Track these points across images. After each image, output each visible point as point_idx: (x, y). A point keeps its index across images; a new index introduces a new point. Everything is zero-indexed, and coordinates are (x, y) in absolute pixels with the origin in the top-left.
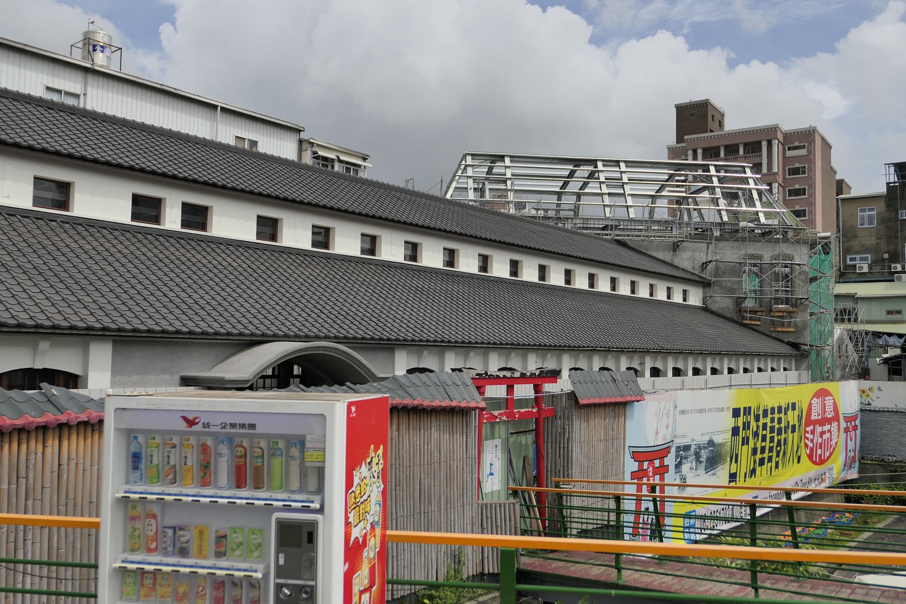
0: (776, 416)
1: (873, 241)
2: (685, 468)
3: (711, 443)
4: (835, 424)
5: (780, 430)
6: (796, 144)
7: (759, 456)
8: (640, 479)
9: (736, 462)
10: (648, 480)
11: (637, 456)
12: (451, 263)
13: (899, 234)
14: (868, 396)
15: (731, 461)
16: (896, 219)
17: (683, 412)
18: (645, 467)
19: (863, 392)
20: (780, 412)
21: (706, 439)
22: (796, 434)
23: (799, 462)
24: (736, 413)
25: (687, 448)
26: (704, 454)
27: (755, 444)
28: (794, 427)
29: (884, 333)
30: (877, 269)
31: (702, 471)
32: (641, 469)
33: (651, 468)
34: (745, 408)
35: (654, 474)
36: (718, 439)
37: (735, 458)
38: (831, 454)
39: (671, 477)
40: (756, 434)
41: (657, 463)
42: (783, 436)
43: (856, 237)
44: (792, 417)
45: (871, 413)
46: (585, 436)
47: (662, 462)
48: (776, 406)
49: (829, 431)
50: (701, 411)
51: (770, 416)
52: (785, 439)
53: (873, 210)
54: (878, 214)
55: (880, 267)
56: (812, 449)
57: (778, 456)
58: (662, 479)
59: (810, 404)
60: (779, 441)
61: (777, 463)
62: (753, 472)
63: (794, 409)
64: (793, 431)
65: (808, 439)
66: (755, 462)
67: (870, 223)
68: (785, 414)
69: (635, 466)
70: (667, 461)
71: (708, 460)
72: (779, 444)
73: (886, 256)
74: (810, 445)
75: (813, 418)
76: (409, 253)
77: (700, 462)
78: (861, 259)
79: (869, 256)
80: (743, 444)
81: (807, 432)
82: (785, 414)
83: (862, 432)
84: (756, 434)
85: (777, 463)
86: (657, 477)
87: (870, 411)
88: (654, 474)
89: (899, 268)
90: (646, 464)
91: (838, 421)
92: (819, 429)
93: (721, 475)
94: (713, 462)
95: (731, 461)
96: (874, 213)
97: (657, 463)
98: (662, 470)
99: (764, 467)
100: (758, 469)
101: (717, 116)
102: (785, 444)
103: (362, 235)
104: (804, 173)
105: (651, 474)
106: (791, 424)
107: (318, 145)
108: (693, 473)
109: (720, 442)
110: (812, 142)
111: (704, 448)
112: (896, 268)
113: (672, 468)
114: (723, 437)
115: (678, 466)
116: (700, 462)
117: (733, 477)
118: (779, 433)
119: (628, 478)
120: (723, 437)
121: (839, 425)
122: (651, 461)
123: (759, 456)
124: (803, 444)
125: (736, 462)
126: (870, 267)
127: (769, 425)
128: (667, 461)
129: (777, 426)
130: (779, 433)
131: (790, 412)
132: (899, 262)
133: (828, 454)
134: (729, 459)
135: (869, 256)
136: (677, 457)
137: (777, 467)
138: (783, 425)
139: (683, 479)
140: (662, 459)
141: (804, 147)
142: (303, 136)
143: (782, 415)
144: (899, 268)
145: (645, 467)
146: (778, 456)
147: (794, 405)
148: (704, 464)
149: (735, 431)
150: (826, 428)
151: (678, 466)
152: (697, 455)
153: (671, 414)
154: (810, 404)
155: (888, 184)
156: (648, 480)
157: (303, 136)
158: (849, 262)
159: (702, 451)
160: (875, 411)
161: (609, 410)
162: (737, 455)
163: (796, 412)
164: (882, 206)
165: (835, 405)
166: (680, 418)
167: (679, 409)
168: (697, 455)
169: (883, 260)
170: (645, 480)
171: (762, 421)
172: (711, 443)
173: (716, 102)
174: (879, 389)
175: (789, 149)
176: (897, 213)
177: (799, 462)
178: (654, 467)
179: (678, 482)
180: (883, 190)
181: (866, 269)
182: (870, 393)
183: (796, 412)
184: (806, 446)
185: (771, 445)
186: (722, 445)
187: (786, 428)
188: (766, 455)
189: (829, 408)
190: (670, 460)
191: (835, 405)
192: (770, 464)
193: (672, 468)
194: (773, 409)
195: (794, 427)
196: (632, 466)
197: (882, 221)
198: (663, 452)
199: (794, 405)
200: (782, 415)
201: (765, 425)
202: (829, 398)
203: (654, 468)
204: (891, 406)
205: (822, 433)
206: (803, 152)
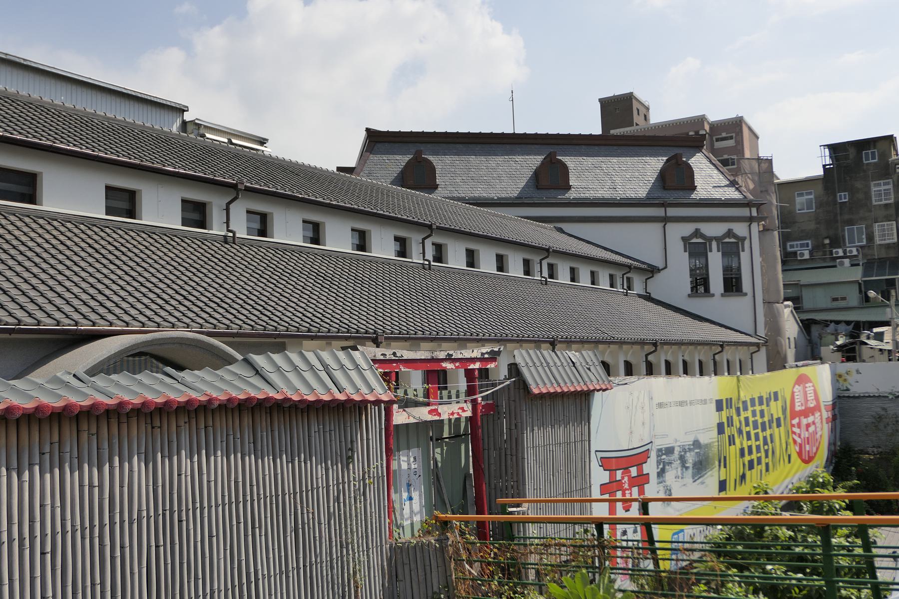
0: (758, 408)
1: (812, 226)
2: (670, 476)
3: (696, 444)
4: (817, 414)
5: (763, 424)
6: (724, 135)
7: (747, 458)
8: (612, 493)
9: (725, 466)
10: (624, 494)
11: (606, 463)
12: (362, 246)
13: (839, 218)
14: (845, 380)
15: (720, 466)
16: (835, 201)
17: (660, 405)
18: (619, 477)
19: (840, 376)
20: (761, 403)
21: (689, 440)
22: (782, 428)
23: (789, 462)
24: (719, 406)
25: (670, 451)
26: (690, 458)
27: (742, 444)
28: (778, 420)
29: (831, 321)
30: (818, 255)
31: (688, 479)
32: (613, 481)
33: (626, 479)
34: (727, 400)
35: (631, 486)
36: (704, 440)
37: (723, 462)
38: (817, 449)
39: (652, 490)
40: (740, 432)
41: (634, 471)
42: (768, 432)
43: (795, 222)
44: (775, 409)
45: (851, 400)
46: (539, 444)
47: (640, 470)
48: (756, 396)
49: (814, 423)
50: (681, 404)
51: (750, 409)
52: (771, 435)
53: (810, 193)
54: (815, 197)
55: (821, 253)
56: (801, 445)
57: (767, 456)
58: (641, 492)
59: (793, 393)
60: (765, 438)
61: (767, 465)
62: (743, 477)
63: (776, 399)
64: (779, 425)
65: (794, 433)
66: (744, 465)
67: (867, 154)
68: (768, 405)
69: (605, 477)
70: (646, 469)
71: (695, 465)
72: (765, 443)
73: (827, 241)
74: (799, 440)
75: (798, 408)
76: (310, 234)
77: (687, 468)
78: (802, 245)
79: (809, 242)
80: (730, 445)
81: (793, 426)
82: (768, 405)
83: (841, 422)
84: (740, 432)
85: (767, 465)
86: (635, 490)
87: (849, 397)
88: (631, 486)
89: (841, 254)
90: (619, 474)
91: (820, 411)
92: (804, 421)
93: (709, 485)
94: (701, 467)
95: (720, 466)
96: (812, 197)
97: (634, 471)
98: (642, 480)
99: (754, 471)
100: (748, 473)
101: (643, 111)
102: (772, 442)
103: (248, 212)
104: (733, 164)
105: (626, 486)
106: (775, 417)
107: (205, 126)
108: (680, 483)
109: (706, 442)
110: (741, 132)
111: (690, 450)
112: (837, 253)
113: (653, 477)
114: (709, 437)
115: (661, 473)
116: (687, 468)
117: (723, 486)
118: (764, 429)
119: (596, 493)
120: (709, 437)
121: (821, 415)
122: (626, 470)
123: (747, 458)
124: (791, 440)
125: (725, 466)
126: (811, 253)
127: (751, 419)
128: (646, 469)
129: (760, 421)
130: (764, 429)
131: (772, 403)
132: (839, 247)
133: (814, 449)
134: (717, 463)
135: (809, 242)
136: (658, 463)
137: (767, 470)
138: (766, 419)
139: (668, 491)
140: (639, 466)
141: (731, 138)
142: (188, 117)
143: (764, 407)
144: (841, 254)
145: (619, 477)
146: (767, 456)
147: (776, 394)
148: (690, 471)
149: (721, 428)
150: (810, 419)
151: (661, 473)
152: (682, 459)
153: (647, 408)
154: (793, 393)
155: (824, 166)
156: (624, 494)
157: (188, 117)
158: (789, 249)
159: (688, 454)
160: (854, 397)
161: (136, 431)
162: (725, 458)
163: (780, 403)
164: (820, 187)
165: (815, 391)
166: (658, 412)
167: (656, 400)
168: (682, 459)
169: (824, 245)
170: (619, 495)
171: (743, 415)
172: (696, 444)
173: (639, 94)
174: (858, 372)
175: (717, 140)
176: (835, 196)
177: (789, 462)
178: (629, 477)
179: (662, 495)
180: (820, 172)
181: (807, 256)
182: (848, 377)
183: (780, 403)
184: (795, 442)
185: (758, 443)
186: (708, 446)
187: (771, 422)
188: (754, 456)
189: (811, 397)
190: (651, 467)
191: (815, 391)
192: (759, 467)
193: (653, 477)
194: (753, 400)
195: (778, 420)
196: (599, 476)
197: (820, 205)
198: (640, 458)
199: (776, 394)
200: (764, 407)
201: (747, 419)
202: (810, 384)
203: (631, 479)
204: (871, 390)
205: (808, 426)
206: (731, 143)
